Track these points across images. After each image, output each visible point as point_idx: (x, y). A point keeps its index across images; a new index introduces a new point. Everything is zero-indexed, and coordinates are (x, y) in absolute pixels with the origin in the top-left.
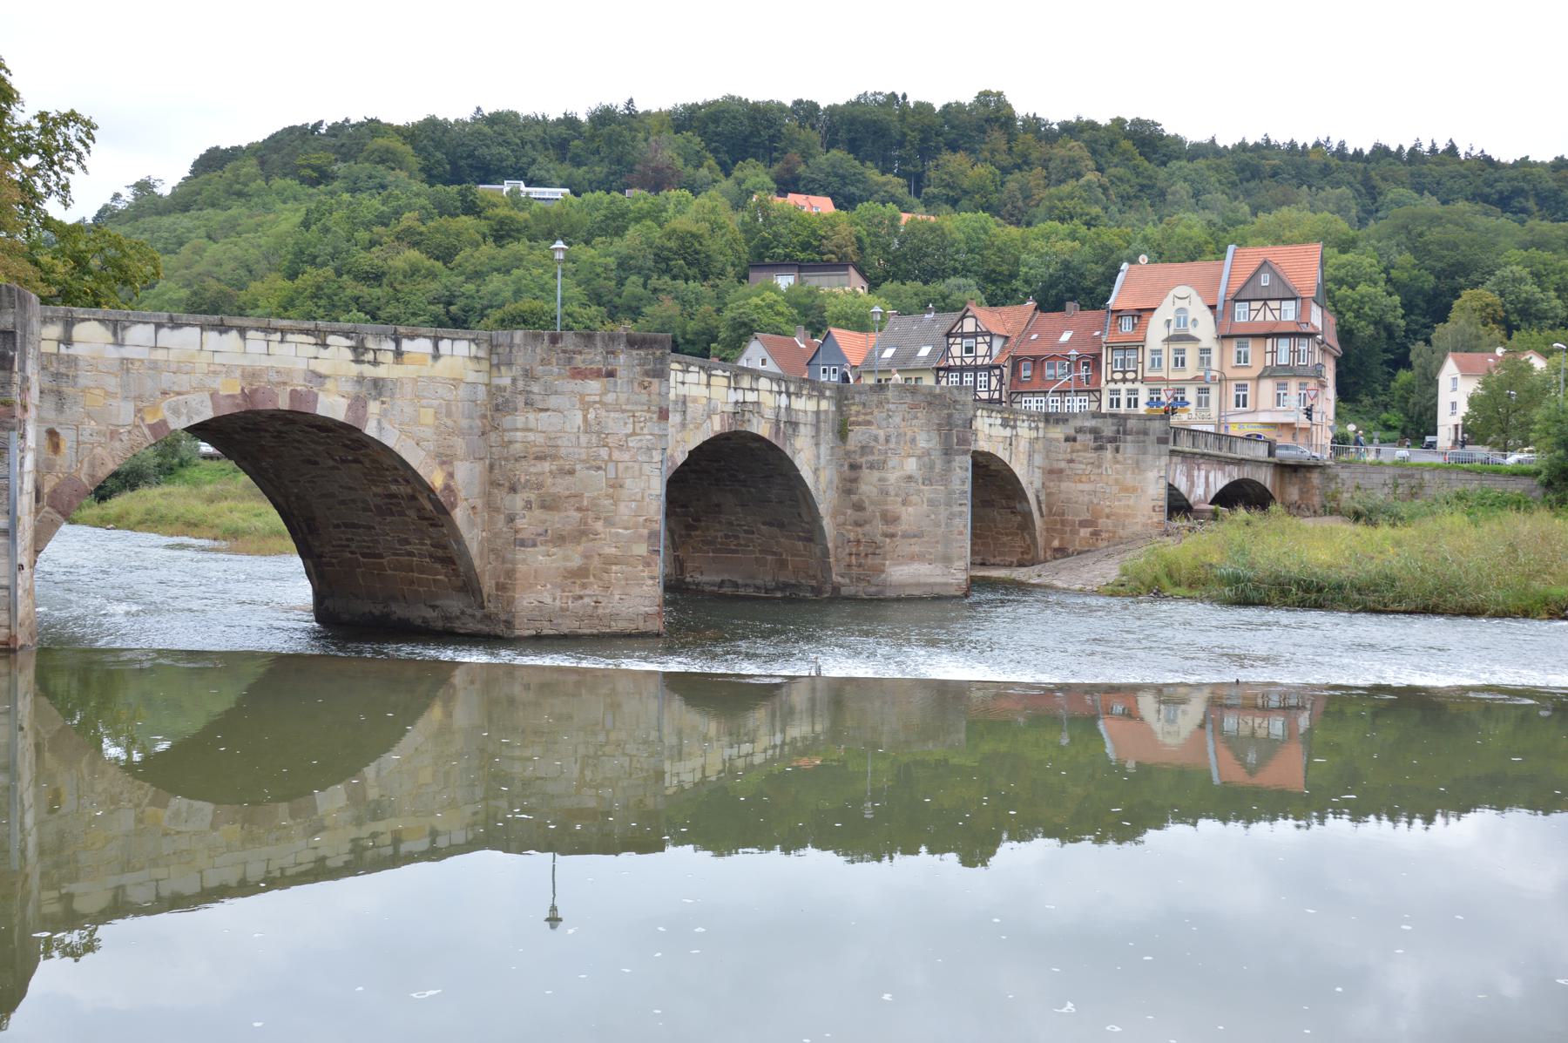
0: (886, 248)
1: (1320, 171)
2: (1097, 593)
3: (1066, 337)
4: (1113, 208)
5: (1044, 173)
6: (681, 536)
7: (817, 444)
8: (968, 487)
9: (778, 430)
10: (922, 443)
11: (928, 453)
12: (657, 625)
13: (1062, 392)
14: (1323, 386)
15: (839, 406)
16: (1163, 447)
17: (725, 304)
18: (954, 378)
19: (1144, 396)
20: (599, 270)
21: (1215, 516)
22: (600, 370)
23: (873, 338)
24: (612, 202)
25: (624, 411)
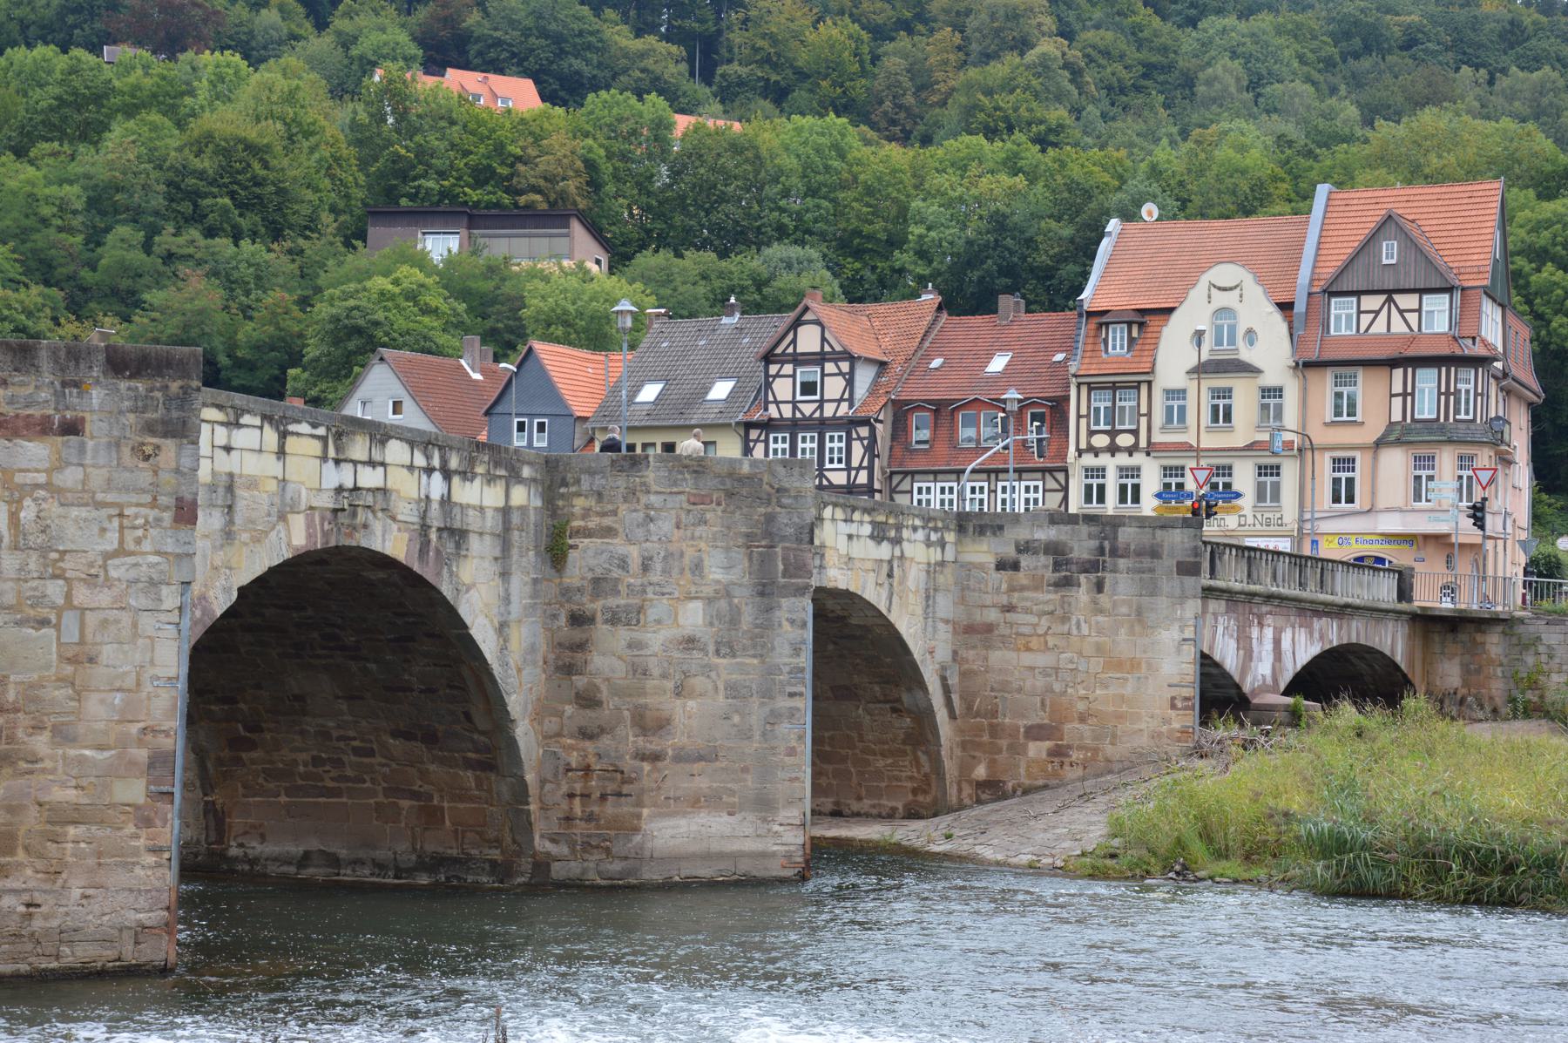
0: (643, 183)
1: (1502, 36)
2: (1062, 872)
3: (998, 364)
4: (1092, 111)
5: (957, 39)
6: (220, 762)
7: (505, 575)
8: (806, 660)
9: (425, 544)
10: (715, 573)
11: (726, 592)
12: (160, 951)
13: (991, 473)
14: (1506, 461)
15: (550, 497)
16: (1190, 581)
17: (318, 290)
18: (779, 444)
19: (1151, 481)
20: (46, 211)
21: (1295, 718)
22: (47, 419)
23: (619, 362)
24: (73, 71)
25: (99, 505)
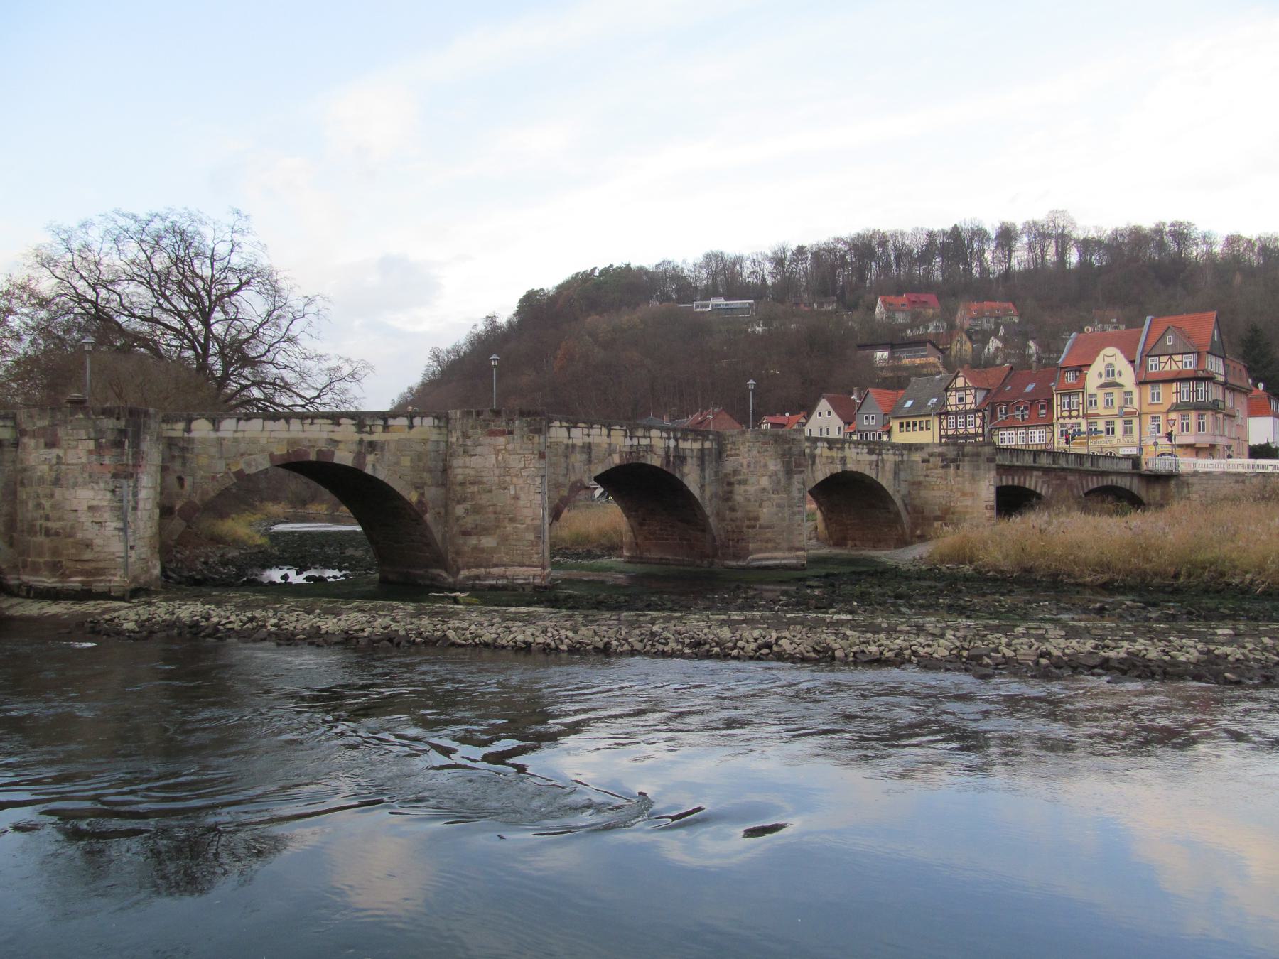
7: (703, 470)
11: (776, 474)
